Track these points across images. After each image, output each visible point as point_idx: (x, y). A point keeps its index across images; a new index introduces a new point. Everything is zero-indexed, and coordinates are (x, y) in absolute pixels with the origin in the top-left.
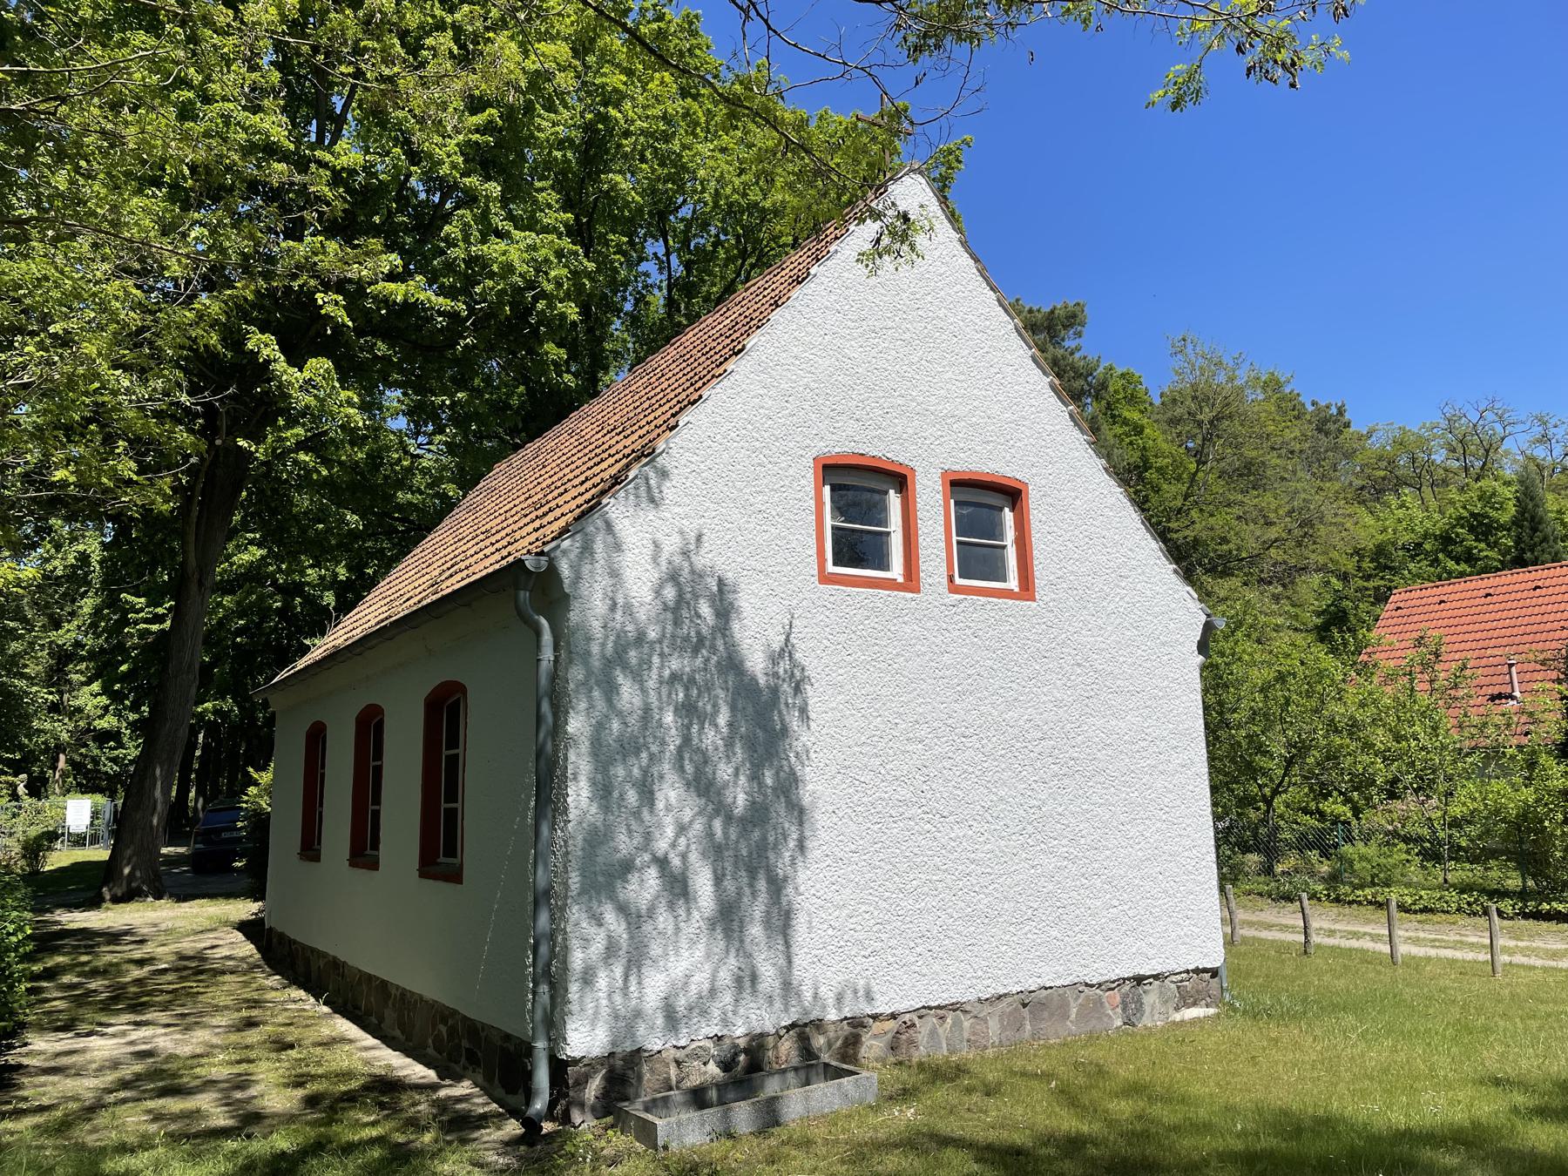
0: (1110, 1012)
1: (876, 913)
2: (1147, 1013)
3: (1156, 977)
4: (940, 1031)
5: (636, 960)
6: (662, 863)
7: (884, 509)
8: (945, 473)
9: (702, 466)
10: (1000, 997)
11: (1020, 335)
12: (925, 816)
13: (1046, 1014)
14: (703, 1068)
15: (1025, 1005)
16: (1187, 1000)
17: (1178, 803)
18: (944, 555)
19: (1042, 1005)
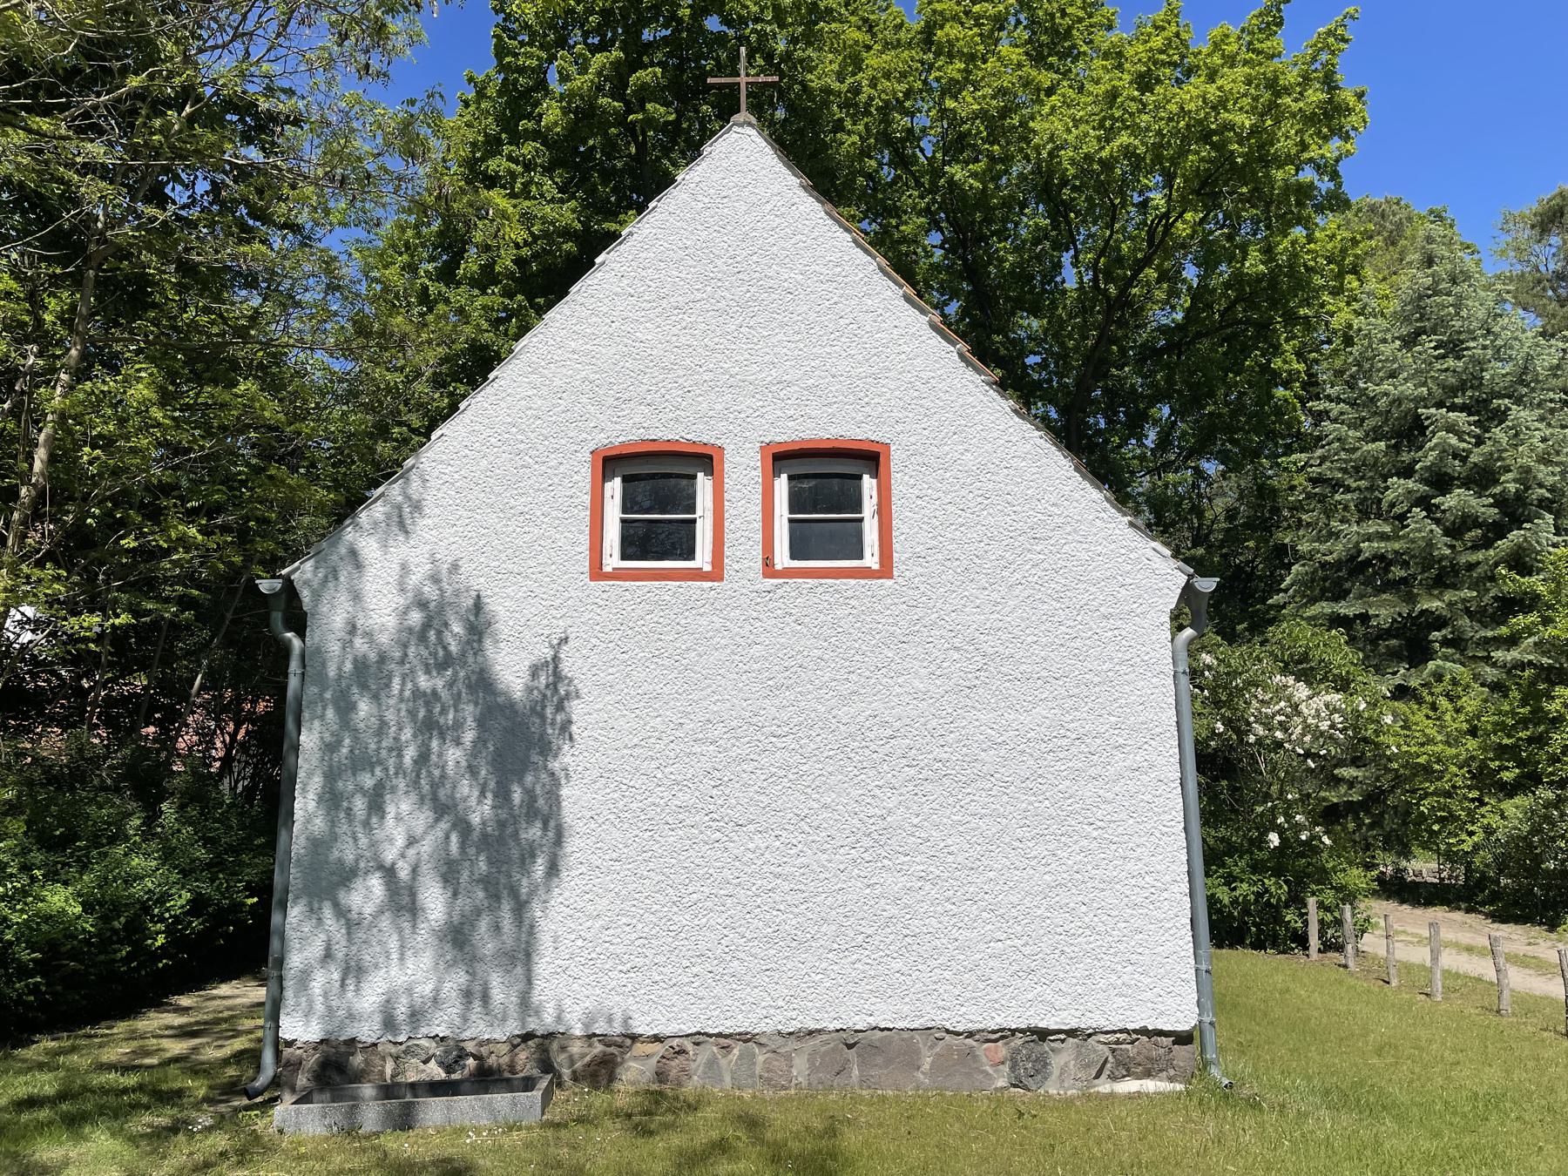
0: (988, 1068)
1: (640, 926)
2: (1054, 1077)
3: (1072, 1033)
4: (723, 1062)
5: (354, 971)
6: (389, 872)
7: (692, 497)
8: (764, 448)
9: (456, 476)
10: (810, 1033)
11: (886, 274)
12: (714, 824)
13: (879, 1060)
14: (422, 1066)
15: (850, 1047)
16: (1126, 1069)
17: (1123, 816)
18: (759, 537)
19: (874, 1048)
